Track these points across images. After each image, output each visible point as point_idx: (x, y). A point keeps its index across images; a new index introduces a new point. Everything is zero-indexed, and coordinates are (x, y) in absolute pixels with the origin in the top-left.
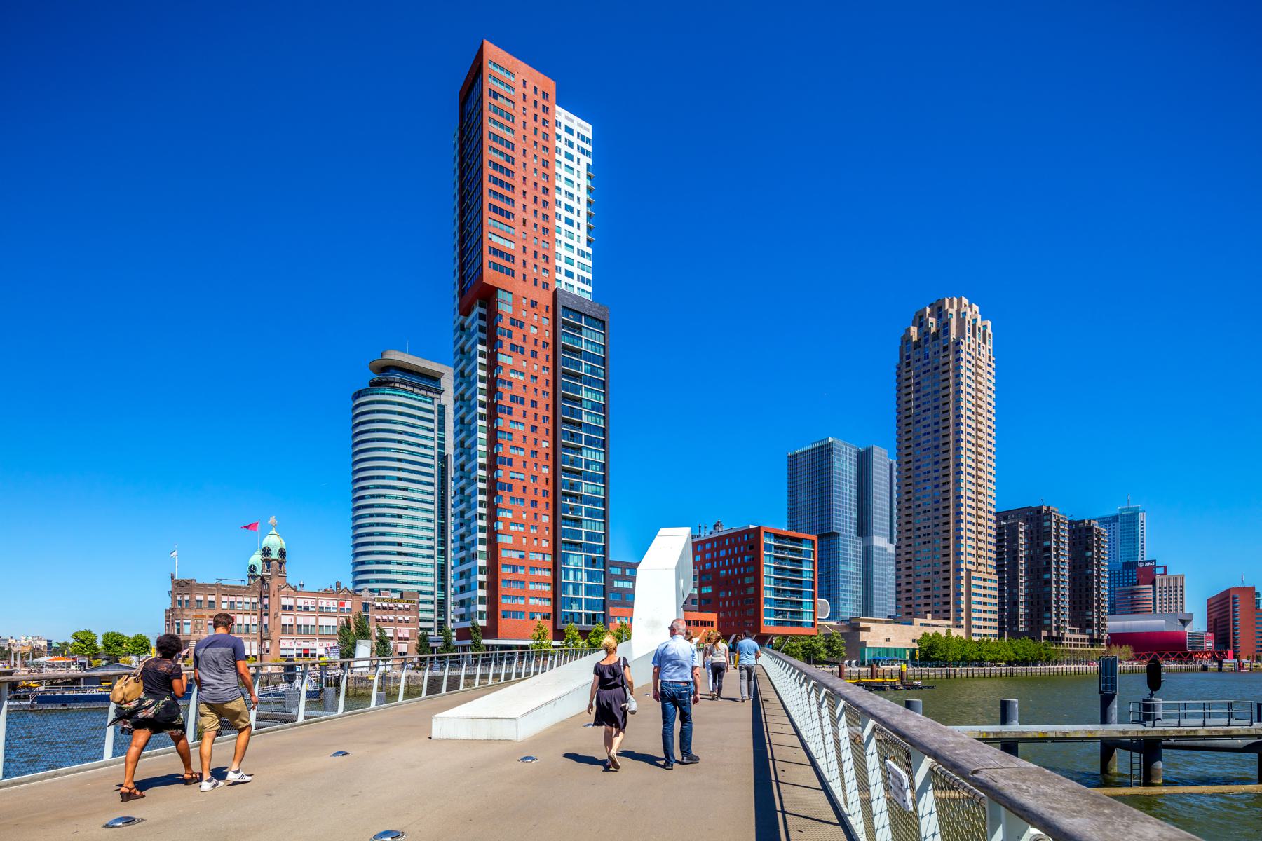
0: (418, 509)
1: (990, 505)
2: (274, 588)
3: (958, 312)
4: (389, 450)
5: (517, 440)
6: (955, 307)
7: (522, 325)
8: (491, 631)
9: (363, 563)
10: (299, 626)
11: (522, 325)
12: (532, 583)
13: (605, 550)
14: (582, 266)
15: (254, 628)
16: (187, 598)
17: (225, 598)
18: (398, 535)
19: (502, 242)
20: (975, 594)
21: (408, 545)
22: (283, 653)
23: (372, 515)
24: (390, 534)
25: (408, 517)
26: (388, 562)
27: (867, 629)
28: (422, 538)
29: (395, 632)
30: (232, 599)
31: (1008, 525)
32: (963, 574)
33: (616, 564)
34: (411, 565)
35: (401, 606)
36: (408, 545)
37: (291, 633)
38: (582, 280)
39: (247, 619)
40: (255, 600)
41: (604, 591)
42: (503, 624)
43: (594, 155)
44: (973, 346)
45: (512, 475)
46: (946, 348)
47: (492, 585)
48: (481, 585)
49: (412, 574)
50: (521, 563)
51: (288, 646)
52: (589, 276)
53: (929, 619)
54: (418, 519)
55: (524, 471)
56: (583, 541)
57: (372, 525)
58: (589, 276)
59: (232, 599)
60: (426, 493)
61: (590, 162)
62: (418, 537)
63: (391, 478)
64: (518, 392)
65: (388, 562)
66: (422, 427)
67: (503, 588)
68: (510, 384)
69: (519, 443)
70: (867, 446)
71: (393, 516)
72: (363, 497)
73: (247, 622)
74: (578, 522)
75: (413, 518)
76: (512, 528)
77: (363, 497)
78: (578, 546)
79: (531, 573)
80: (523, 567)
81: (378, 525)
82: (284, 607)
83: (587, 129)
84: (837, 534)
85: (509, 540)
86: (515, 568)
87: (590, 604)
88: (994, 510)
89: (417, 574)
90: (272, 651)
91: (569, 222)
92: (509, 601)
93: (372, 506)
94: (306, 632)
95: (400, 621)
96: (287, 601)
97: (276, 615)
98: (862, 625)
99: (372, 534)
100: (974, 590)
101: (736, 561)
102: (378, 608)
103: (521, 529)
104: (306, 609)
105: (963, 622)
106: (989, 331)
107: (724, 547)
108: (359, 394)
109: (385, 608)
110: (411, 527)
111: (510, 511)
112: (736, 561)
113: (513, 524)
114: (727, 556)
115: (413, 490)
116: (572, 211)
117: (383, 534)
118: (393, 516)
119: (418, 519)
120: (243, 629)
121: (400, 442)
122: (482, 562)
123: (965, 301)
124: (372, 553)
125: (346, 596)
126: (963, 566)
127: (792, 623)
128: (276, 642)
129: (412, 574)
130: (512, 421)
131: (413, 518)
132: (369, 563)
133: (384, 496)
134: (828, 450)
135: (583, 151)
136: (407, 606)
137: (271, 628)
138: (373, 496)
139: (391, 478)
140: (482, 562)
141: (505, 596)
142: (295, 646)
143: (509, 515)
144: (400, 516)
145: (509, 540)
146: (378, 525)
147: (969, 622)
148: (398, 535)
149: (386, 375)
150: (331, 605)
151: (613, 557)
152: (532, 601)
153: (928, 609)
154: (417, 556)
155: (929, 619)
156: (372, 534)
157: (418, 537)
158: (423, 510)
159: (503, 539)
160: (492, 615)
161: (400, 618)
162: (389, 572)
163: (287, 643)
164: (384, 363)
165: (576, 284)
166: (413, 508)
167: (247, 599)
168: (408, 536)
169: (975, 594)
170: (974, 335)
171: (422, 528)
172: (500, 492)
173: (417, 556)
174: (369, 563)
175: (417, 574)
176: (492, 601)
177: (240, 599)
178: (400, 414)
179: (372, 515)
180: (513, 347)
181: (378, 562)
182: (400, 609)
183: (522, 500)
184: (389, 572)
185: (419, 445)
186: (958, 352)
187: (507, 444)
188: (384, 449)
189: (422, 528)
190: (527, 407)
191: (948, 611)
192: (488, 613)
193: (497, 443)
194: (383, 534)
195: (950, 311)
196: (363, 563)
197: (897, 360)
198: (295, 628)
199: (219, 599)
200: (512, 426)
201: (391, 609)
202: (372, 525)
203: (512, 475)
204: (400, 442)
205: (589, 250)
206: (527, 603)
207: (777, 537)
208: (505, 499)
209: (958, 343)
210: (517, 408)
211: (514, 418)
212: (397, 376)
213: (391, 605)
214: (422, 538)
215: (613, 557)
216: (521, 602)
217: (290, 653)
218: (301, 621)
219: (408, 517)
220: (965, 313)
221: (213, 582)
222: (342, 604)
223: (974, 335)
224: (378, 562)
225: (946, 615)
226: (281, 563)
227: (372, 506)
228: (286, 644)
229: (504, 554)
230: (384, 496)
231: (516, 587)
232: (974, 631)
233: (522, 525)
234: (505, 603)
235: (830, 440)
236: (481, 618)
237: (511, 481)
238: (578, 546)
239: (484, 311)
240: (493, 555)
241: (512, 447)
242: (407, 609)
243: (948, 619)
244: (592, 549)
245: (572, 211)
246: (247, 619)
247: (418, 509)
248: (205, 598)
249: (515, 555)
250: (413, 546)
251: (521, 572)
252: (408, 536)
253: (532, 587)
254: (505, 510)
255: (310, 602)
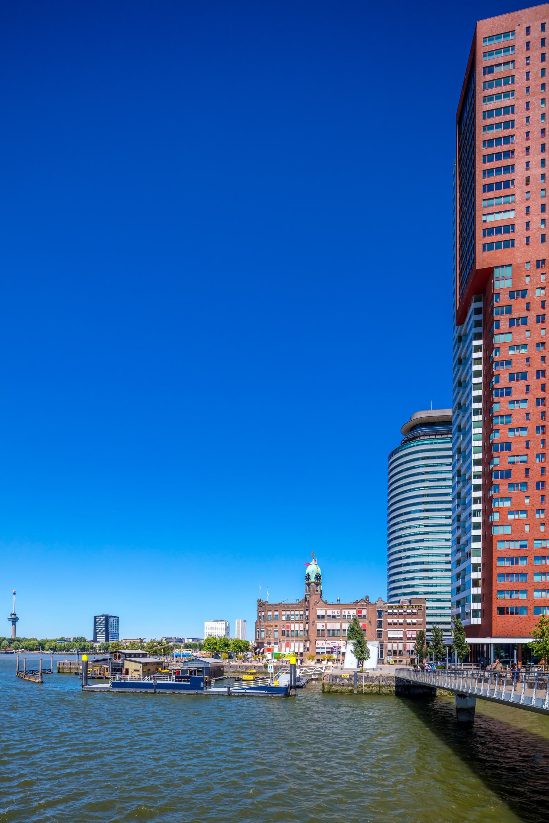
0: (437, 532)
2: (312, 602)
4: (414, 490)
5: (518, 420)
7: (524, 293)
8: (485, 630)
9: (394, 582)
10: (329, 630)
11: (524, 293)
12: (537, 574)
15: (302, 633)
16: (263, 614)
17: (284, 613)
18: (419, 556)
19: (498, 217)
21: (428, 563)
22: (318, 650)
23: (400, 544)
24: (414, 556)
25: (428, 540)
26: (413, 579)
28: (440, 555)
29: (404, 633)
30: (288, 613)
34: (431, 578)
35: (409, 611)
36: (428, 563)
37: (323, 636)
39: (297, 627)
40: (302, 613)
42: (498, 621)
45: (511, 459)
47: (487, 582)
48: (476, 583)
49: (432, 586)
50: (523, 553)
51: (321, 646)
54: (437, 540)
55: (528, 451)
57: (400, 551)
59: (288, 613)
60: (443, 518)
62: (437, 555)
63: (415, 512)
64: (518, 367)
65: (413, 579)
66: (441, 464)
67: (498, 583)
68: (509, 362)
69: (522, 423)
71: (416, 541)
72: (394, 532)
73: (297, 629)
75: (433, 540)
76: (511, 517)
77: (394, 532)
79: (537, 563)
80: (524, 558)
81: (405, 550)
82: (319, 617)
85: (507, 530)
86: (514, 560)
89: (436, 585)
90: (310, 649)
92: (507, 596)
93: (401, 537)
94: (334, 635)
95: (409, 624)
96: (320, 613)
97: (313, 622)
99: (400, 558)
102: (390, 614)
103: (523, 516)
104: (334, 617)
109: (395, 614)
110: (432, 548)
111: (509, 499)
113: (511, 512)
115: (433, 518)
117: (408, 557)
118: (416, 541)
119: (437, 540)
120: (295, 632)
121: (423, 481)
122: (477, 560)
124: (400, 573)
125: (362, 606)
128: (313, 642)
129: (432, 586)
130: (511, 402)
131: (433, 540)
132: (398, 581)
133: (410, 527)
136: (415, 611)
137: (310, 632)
138: (401, 529)
139: (415, 512)
140: (477, 560)
141: (501, 592)
142: (326, 646)
143: (508, 504)
144: (422, 541)
145: (507, 530)
146: (405, 550)
148: (419, 556)
149: (414, 431)
150: (351, 614)
152: (537, 595)
154: (437, 570)
156: (400, 558)
157: (437, 555)
158: (441, 532)
159: (497, 531)
160: (486, 613)
161: (395, 621)
162: (413, 586)
163: (321, 643)
164: (412, 423)
166: (433, 532)
167: (297, 613)
168: (428, 555)
171: (441, 547)
172: (495, 481)
173: (437, 570)
174: (398, 581)
175: (436, 585)
176: (487, 598)
177: (293, 613)
178: (423, 458)
179: (400, 544)
180: (512, 322)
181: (405, 580)
182: (409, 614)
183: (524, 484)
184: (413, 586)
185: (439, 480)
187: (504, 430)
188: (410, 490)
189: (441, 547)
190: (533, 380)
192: (483, 611)
193: (492, 430)
194: (408, 557)
196: (394, 582)
198: (326, 632)
199: (280, 613)
200: (511, 407)
201: (401, 614)
202: (400, 551)
203: (511, 459)
204: (423, 481)
206: (530, 597)
208: (502, 487)
210: (519, 386)
211: (514, 397)
212: (422, 431)
213: (401, 611)
214: (440, 555)
216: (523, 596)
217: (323, 650)
218: (330, 626)
219: (428, 540)
222: (360, 612)
224: (405, 580)
226: (317, 585)
227: (401, 537)
228: (320, 644)
229: (501, 546)
230: (410, 527)
231: (516, 582)
233: (524, 512)
234: (501, 599)
236: (475, 616)
237: (508, 467)
239: (480, 305)
240: (488, 551)
241: (511, 430)
242: (415, 614)
246: (297, 627)
247: (437, 532)
249: (515, 546)
250: (433, 563)
251: (522, 563)
252: (428, 555)
253: (537, 579)
254: (502, 499)
255: (336, 612)
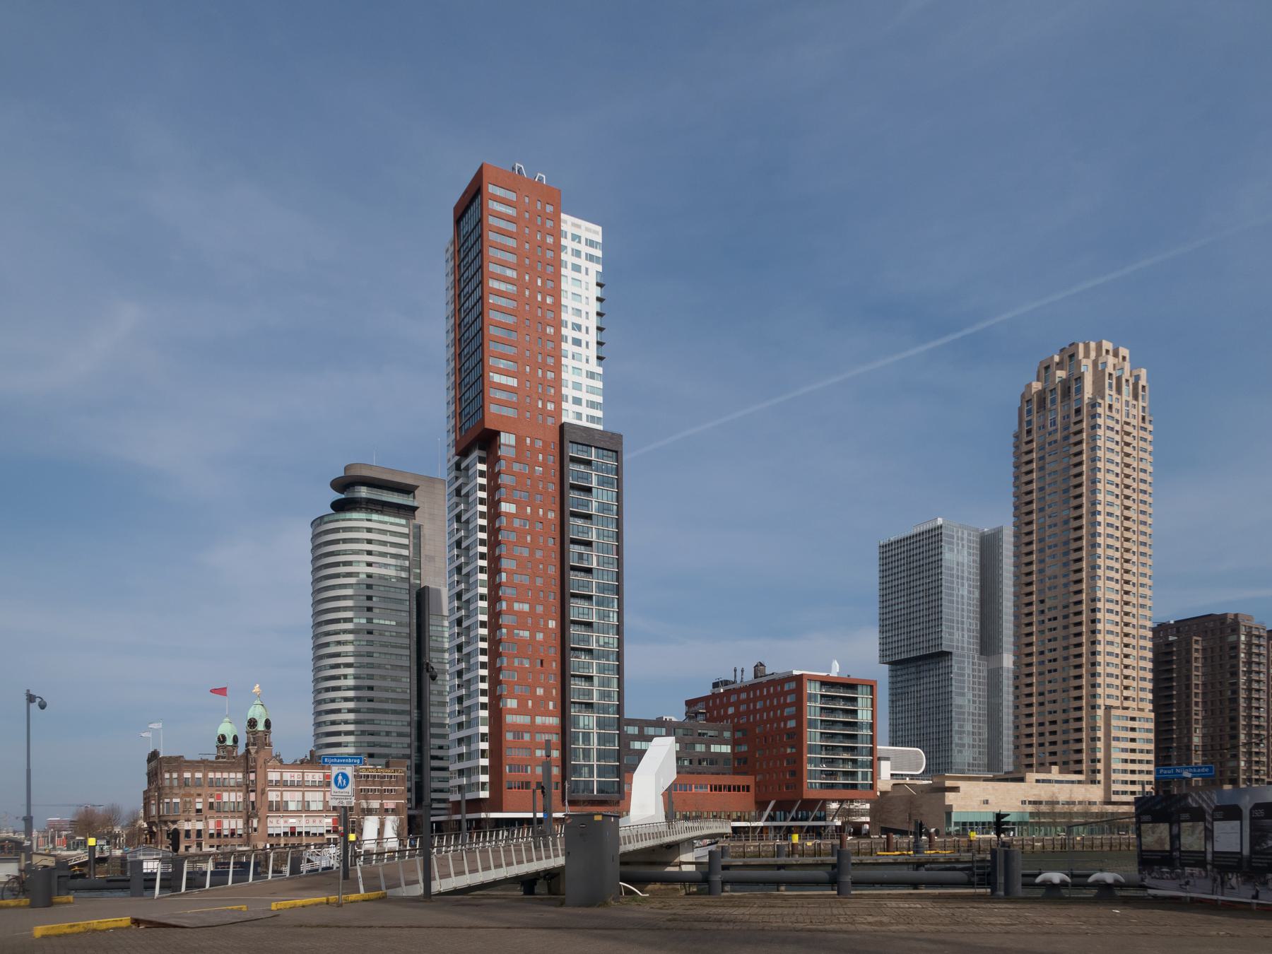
1: (1144, 622)
3: (1095, 363)
6: (1093, 354)
8: (495, 803)
13: (620, 709)
14: (591, 390)
20: (1117, 739)
27: (955, 789)
31: (1178, 642)
32: (1100, 712)
33: (632, 722)
38: (592, 405)
41: (619, 755)
42: (509, 796)
43: (605, 261)
44: (1116, 405)
46: (1078, 411)
52: (599, 399)
53: (1055, 773)
56: (595, 565)
58: (599, 399)
61: (600, 268)
70: (995, 525)
74: (588, 490)
78: (589, 706)
83: (596, 233)
84: (947, 655)
87: (602, 771)
88: (1149, 624)
90: (260, 830)
91: (577, 342)
98: (948, 783)
100: (1114, 733)
101: (775, 714)
105: (1100, 777)
106: (1143, 382)
107: (762, 698)
108: (319, 521)
112: (775, 714)
114: (765, 709)
116: (580, 329)
123: (1107, 345)
126: (1100, 701)
127: (845, 786)
134: (933, 538)
135: (590, 258)
137: (258, 805)
147: (1107, 777)
151: (628, 714)
153: (1053, 759)
155: (1055, 773)
165: (585, 411)
169: (1117, 739)
170: (1119, 391)
186: (1094, 416)
191: (1079, 762)
195: (1084, 362)
197: (1016, 428)
205: (600, 370)
207: (825, 683)
209: (1094, 405)
215: (628, 714)
220: (1105, 364)
221: (198, 758)
223: (1119, 391)
225: (1077, 767)
229: (509, 719)
232: (1115, 787)
235: (940, 521)
238: (589, 706)
243: (1080, 772)
244: (605, 709)
245: (580, 329)
248: (205, 776)
